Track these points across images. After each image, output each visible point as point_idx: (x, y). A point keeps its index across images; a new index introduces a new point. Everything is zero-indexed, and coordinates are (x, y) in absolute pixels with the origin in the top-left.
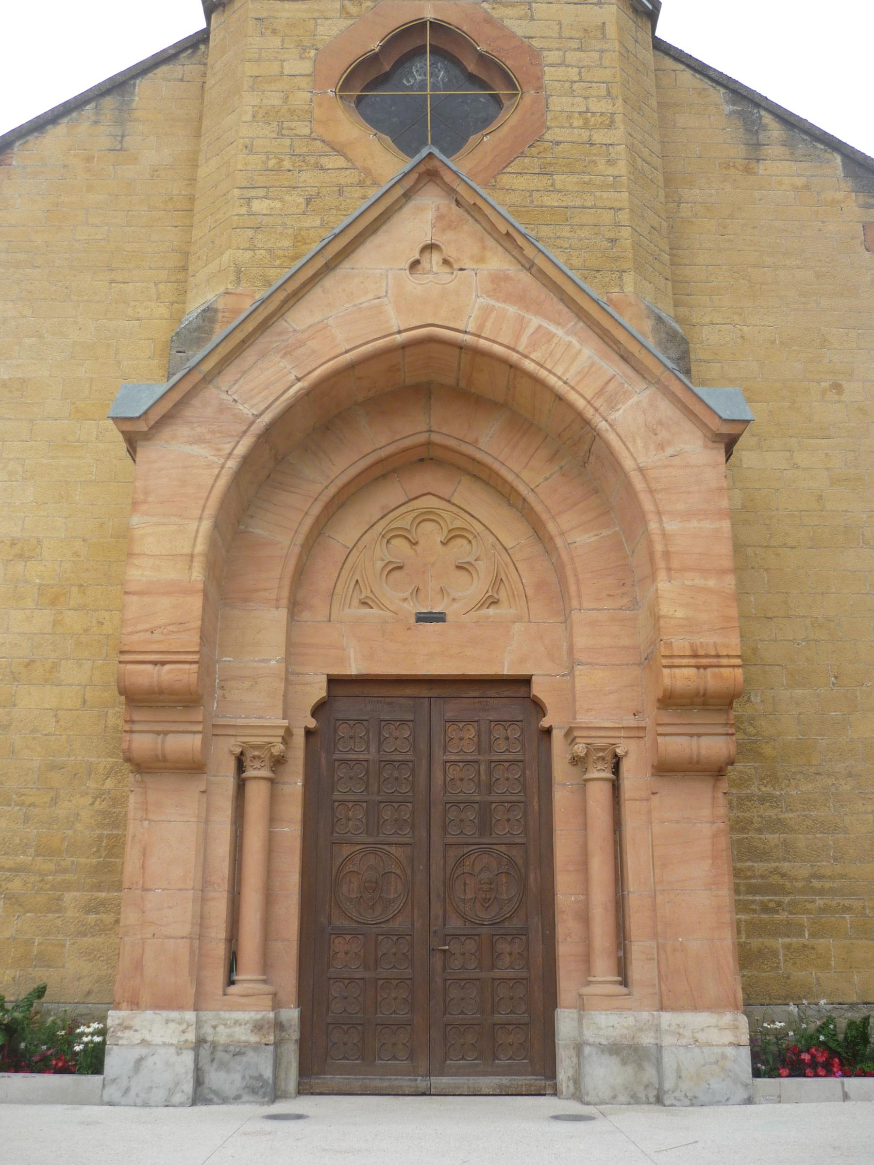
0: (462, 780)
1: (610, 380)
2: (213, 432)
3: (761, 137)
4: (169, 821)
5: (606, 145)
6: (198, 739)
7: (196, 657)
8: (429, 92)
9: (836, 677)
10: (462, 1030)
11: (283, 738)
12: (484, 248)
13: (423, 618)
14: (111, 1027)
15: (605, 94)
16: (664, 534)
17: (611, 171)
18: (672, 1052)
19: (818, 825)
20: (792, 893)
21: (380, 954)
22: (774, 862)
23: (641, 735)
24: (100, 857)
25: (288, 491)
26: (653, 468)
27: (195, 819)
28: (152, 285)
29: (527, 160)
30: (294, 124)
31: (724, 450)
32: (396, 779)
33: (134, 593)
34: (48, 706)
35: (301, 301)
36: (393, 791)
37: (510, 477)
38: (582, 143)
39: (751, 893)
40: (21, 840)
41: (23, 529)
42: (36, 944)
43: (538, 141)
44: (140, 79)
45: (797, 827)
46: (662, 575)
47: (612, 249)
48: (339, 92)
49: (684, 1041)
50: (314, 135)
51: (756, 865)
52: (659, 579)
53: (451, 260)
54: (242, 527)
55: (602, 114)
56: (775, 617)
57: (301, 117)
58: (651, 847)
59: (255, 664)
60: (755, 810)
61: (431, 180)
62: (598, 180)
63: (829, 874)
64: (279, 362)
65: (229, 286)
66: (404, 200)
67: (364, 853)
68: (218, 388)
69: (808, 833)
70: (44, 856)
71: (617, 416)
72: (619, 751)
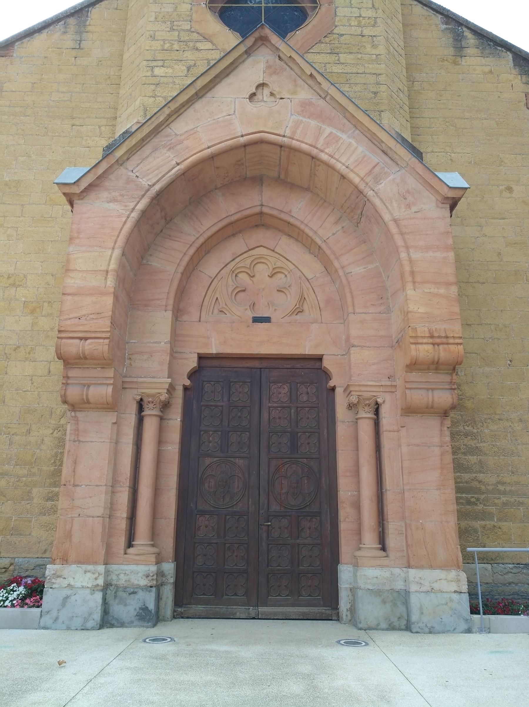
0: (280, 418)
1: (376, 166)
2: (122, 196)
3: (463, 43)
4: (92, 442)
5: (371, 36)
6: (110, 389)
7: (108, 335)
8: (263, 5)
9: (511, 361)
10: (279, 577)
11: (168, 390)
12: (296, 85)
13: (257, 320)
14: (49, 575)
15: (371, 6)
16: (411, 261)
17: (374, 52)
18: (417, 596)
19: (501, 451)
20: (486, 493)
21: (227, 528)
22: (474, 473)
23: (393, 390)
24: (56, 466)
25: (173, 240)
26: (403, 220)
27: (109, 441)
28: (97, 127)
29: (323, 45)
30: (181, 23)
31: (449, 208)
32: (240, 417)
33: (69, 294)
34: (27, 374)
35: (181, 116)
36: (237, 424)
37: (311, 234)
38: (357, 35)
39: (460, 492)
40: (7, 456)
41: (15, 269)
42: (13, 520)
43: (330, 34)
44: (91, 8)
45: (488, 452)
46: (409, 286)
47: (375, 98)
48: (208, 4)
49: (424, 589)
50: (192, 30)
51: (463, 475)
52: (408, 288)
53: (275, 92)
54: (144, 261)
55: (369, 18)
56: (472, 324)
57: (185, 19)
58: (400, 461)
59: (151, 345)
60: (462, 441)
61: (263, 44)
62: (366, 57)
63: (509, 482)
64: (166, 154)
65: (140, 119)
66: (246, 56)
67: (219, 463)
68: (127, 169)
69: (495, 456)
70: (21, 466)
71: (381, 187)
72: (380, 400)
